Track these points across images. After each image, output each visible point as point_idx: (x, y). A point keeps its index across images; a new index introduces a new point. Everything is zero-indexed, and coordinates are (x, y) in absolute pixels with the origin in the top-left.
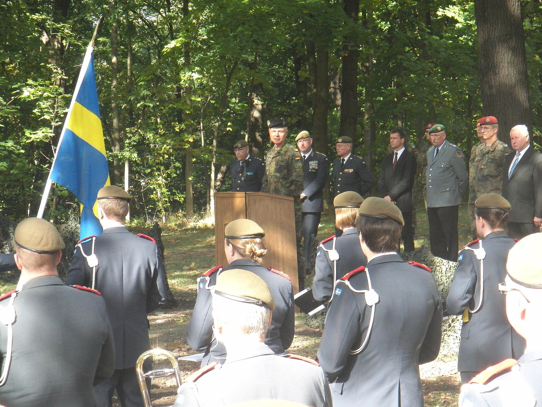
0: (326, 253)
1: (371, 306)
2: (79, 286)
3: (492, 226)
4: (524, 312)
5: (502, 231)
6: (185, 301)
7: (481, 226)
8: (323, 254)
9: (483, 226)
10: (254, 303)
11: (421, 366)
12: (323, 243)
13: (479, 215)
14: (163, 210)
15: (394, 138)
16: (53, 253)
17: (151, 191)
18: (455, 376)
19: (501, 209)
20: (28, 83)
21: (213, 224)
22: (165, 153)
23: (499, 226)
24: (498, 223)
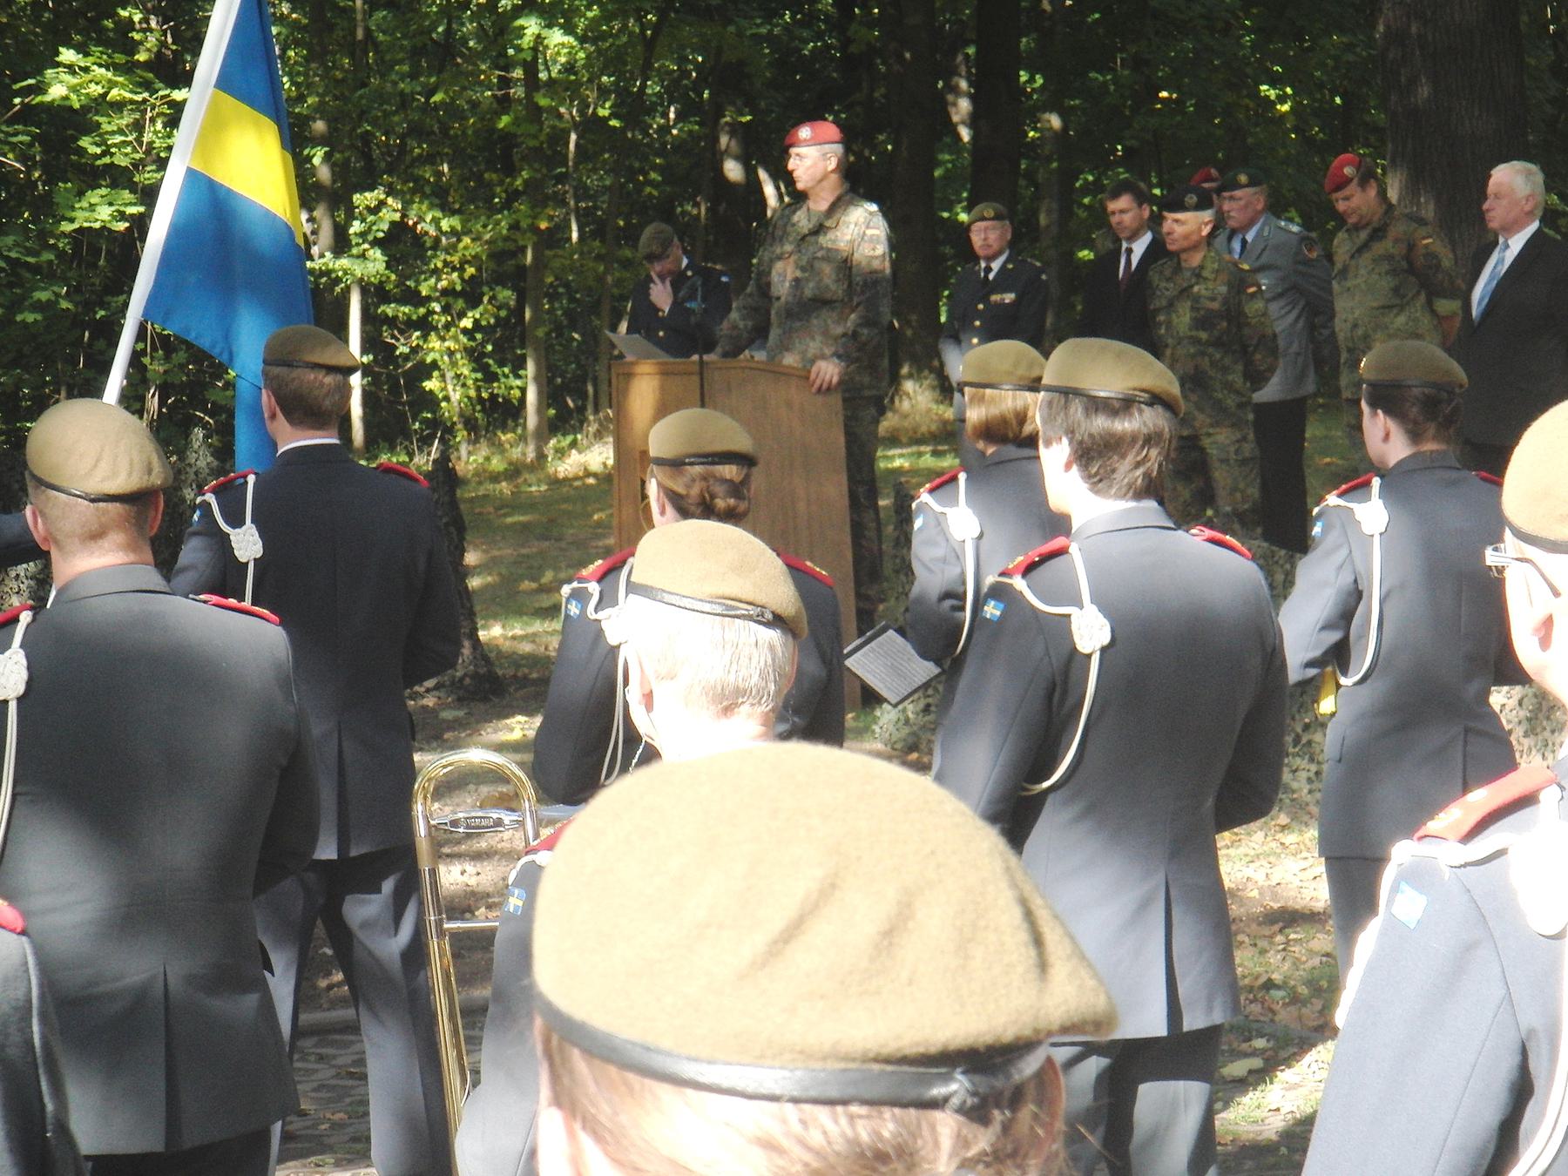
0: (941, 518)
1: (1089, 656)
2: (215, 598)
3: (1415, 436)
4: (1548, 623)
5: (1444, 452)
6: (525, 677)
7: (1381, 434)
8: (932, 522)
9: (1387, 437)
10: (749, 618)
11: (1224, 839)
12: (931, 491)
13: (1374, 405)
14: (459, 426)
15: (1122, 211)
16: (135, 499)
17: (427, 370)
18: (1314, 884)
19: (1434, 385)
20: (60, 59)
21: (605, 465)
22: (468, 262)
23: (1434, 438)
24: (1431, 431)
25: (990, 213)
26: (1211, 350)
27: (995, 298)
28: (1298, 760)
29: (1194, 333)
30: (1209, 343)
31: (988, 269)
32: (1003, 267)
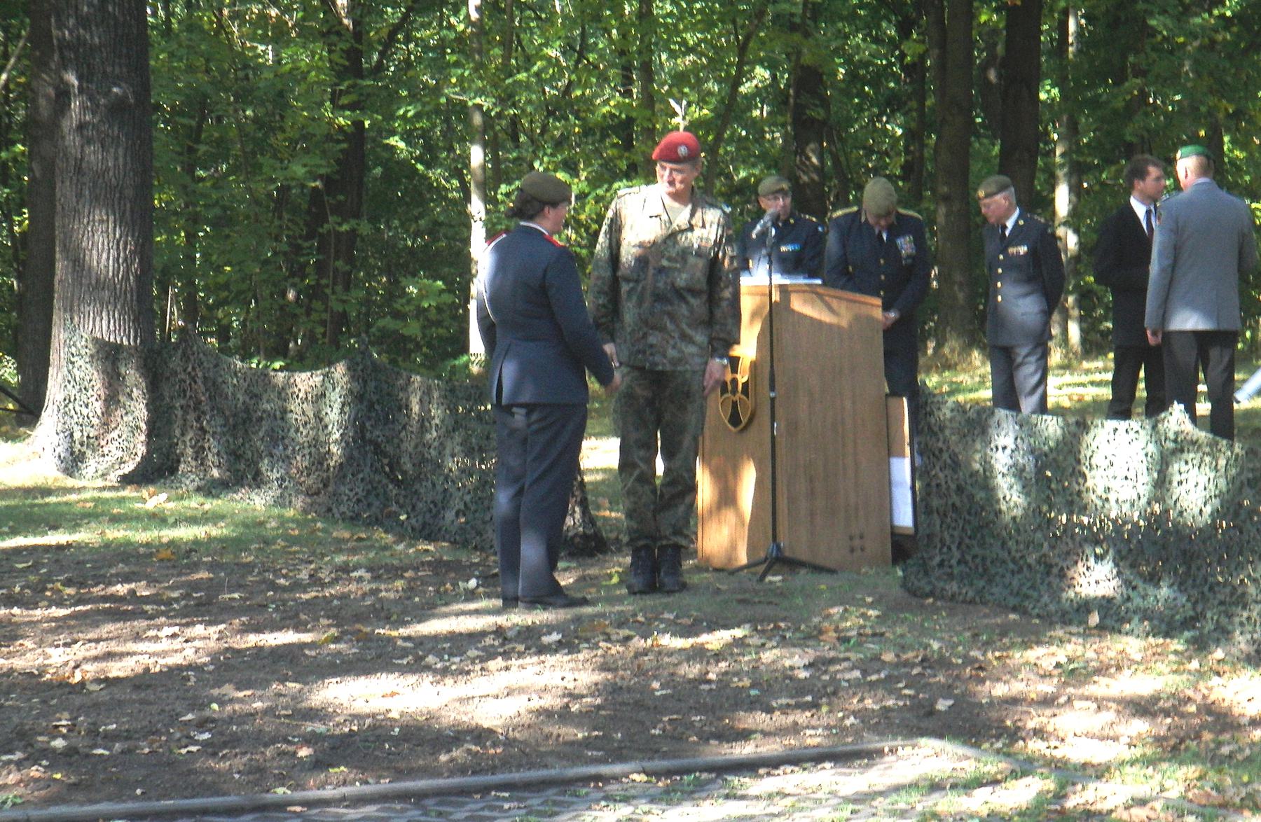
27: (1012, 250)
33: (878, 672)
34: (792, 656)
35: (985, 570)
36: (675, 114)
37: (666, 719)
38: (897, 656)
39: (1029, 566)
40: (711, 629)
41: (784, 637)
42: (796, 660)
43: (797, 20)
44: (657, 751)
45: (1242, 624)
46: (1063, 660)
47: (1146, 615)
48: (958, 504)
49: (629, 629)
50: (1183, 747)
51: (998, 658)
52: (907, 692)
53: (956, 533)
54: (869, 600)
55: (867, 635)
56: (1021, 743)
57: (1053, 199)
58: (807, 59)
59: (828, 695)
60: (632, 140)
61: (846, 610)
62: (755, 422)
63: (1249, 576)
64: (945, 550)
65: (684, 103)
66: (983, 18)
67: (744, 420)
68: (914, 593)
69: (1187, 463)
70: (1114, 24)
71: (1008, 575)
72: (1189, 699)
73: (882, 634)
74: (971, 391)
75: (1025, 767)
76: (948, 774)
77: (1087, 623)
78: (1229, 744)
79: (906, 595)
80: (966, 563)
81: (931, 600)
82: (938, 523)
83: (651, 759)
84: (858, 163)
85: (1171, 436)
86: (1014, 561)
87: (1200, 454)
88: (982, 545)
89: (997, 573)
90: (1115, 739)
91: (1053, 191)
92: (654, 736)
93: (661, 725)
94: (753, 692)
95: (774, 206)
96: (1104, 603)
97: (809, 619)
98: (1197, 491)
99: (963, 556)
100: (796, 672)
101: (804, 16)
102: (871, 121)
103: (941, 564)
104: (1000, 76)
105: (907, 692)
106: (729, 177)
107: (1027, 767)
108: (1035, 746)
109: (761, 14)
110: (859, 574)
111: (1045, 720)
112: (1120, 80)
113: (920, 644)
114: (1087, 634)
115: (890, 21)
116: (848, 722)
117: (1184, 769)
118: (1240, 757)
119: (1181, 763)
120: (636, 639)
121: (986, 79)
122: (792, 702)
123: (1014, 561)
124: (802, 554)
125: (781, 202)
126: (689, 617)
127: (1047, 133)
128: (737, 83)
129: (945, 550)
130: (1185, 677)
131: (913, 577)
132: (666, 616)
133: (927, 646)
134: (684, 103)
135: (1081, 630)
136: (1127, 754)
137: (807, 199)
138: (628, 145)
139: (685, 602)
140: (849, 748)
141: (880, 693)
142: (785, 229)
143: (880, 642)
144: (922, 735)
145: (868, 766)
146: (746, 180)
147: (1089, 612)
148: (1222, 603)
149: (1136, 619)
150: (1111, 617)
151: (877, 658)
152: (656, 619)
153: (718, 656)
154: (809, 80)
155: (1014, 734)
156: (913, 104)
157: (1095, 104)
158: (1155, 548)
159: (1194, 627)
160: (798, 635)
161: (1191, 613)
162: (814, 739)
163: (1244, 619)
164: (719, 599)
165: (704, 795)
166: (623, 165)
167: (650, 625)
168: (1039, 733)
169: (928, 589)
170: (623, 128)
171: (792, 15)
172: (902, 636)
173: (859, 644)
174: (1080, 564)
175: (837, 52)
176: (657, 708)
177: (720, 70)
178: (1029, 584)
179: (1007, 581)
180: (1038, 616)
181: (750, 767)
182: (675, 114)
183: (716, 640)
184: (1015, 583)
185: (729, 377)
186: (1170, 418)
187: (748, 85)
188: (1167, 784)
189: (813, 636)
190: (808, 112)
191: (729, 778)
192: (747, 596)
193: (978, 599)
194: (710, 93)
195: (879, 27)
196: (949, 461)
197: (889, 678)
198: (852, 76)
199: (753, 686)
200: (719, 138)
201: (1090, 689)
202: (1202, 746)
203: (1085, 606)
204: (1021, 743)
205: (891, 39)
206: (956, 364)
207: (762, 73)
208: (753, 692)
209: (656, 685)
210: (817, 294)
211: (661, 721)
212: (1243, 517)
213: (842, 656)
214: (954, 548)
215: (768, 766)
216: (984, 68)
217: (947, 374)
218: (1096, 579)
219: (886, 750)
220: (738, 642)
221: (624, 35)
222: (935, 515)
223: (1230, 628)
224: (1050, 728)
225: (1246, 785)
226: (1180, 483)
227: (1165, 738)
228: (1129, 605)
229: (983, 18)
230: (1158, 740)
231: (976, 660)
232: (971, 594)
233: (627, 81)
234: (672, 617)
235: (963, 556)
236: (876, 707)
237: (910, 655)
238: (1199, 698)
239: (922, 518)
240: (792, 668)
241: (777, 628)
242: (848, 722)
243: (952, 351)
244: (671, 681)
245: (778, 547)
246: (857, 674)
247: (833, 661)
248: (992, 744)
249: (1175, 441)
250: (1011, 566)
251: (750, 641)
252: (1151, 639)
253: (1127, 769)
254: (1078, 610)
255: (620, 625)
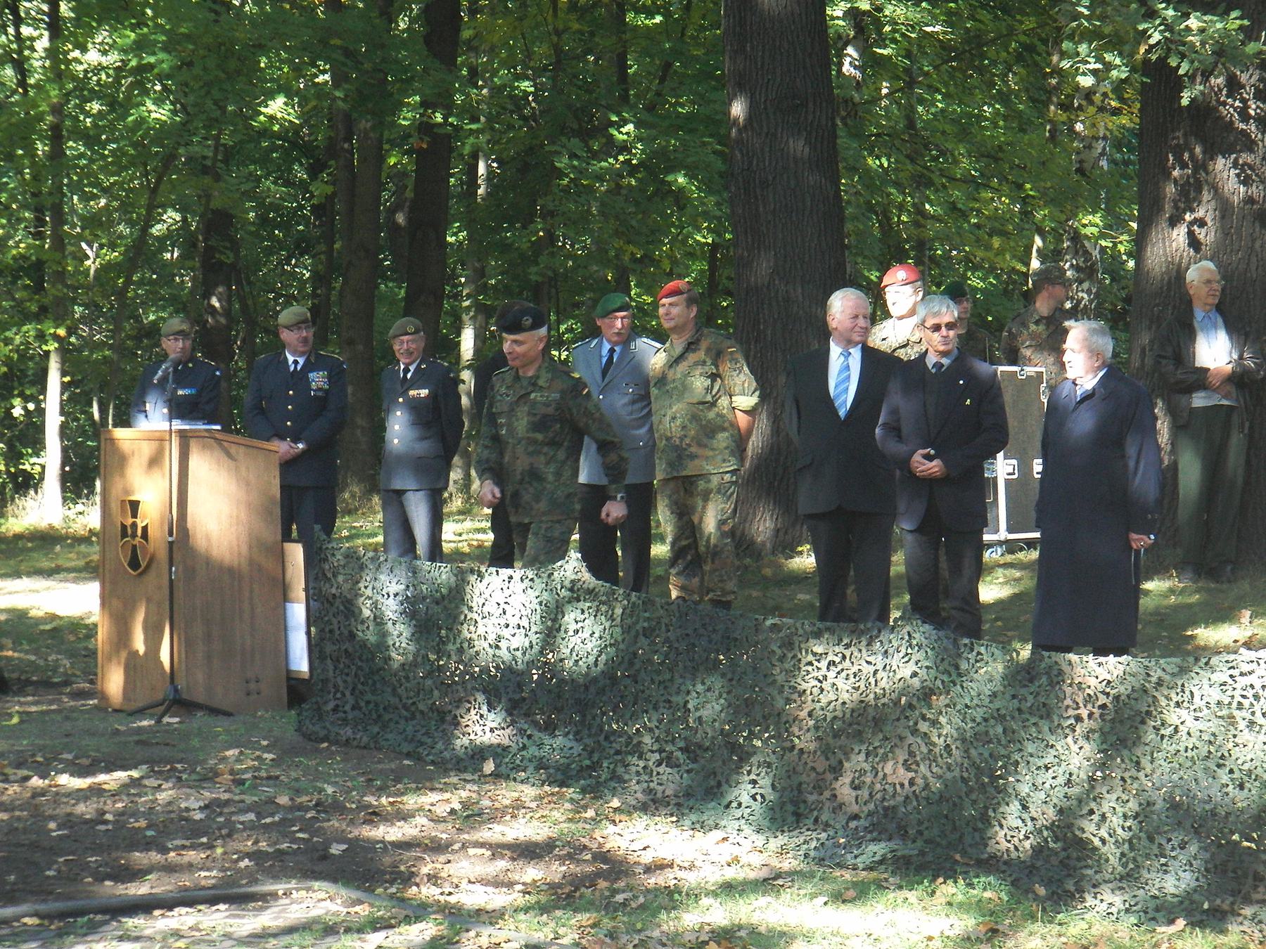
25: (411, 329)
26: (545, 449)
27: (412, 393)
28: (630, 758)
29: (531, 435)
30: (544, 444)
31: (406, 370)
32: (418, 368)
33: (272, 815)
34: (187, 799)
35: (379, 716)
36: (88, 257)
37: (61, 860)
38: (291, 799)
39: (422, 712)
40: (109, 770)
41: (180, 779)
42: (194, 803)
43: (209, 163)
44: (51, 893)
45: (638, 773)
46: (457, 806)
47: (541, 765)
48: (350, 650)
49: (28, 769)
50: (577, 894)
51: (391, 804)
52: (301, 835)
53: (349, 679)
54: (265, 743)
55: (261, 778)
56: (414, 888)
57: (459, 343)
58: (216, 204)
59: (222, 837)
60: (44, 281)
61: (241, 753)
62: (154, 566)
63: (645, 727)
64: (339, 695)
65: (96, 245)
66: (392, 161)
67: (143, 564)
68: (309, 737)
69: (583, 612)
70: (525, 169)
71: (403, 722)
72: (585, 847)
73: (277, 777)
74: (369, 536)
75: (419, 912)
76: (341, 918)
77: (481, 770)
78: (624, 892)
79: (301, 739)
80: (360, 709)
81: (325, 745)
82: (331, 668)
83: (44, 901)
84: (266, 306)
85: (567, 583)
86: (405, 707)
87: (597, 603)
88: (374, 692)
89: (391, 720)
90: (510, 885)
91: (459, 335)
92: (48, 877)
93: (55, 867)
94: (149, 833)
95: (174, 347)
96: (499, 750)
97: (205, 761)
98: (585, 639)
99: (357, 702)
100: (192, 813)
101: (215, 159)
102: (280, 263)
103: (335, 710)
104: (409, 220)
105: (301, 835)
106: (138, 319)
107: (418, 913)
108: (428, 892)
109: (173, 157)
110: (255, 717)
111: (439, 866)
112: (528, 220)
113: (315, 788)
114: (483, 779)
115: (301, 164)
116: (242, 864)
117: (579, 917)
118: (634, 905)
119: (575, 911)
120: (35, 778)
121: (395, 223)
122: (187, 843)
123: (405, 707)
124: (200, 697)
125: (180, 344)
126: (88, 757)
127: (455, 276)
128: (148, 225)
129: (339, 695)
130: (581, 825)
131: (307, 722)
132: (65, 756)
133: (321, 790)
134: (96, 245)
135: (476, 777)
136: (521, 900)
137: (211, 341)
138: (39, 288)
139: (84, 743)
140: (243, 890)
141: (274, 835)
142: (181, 376)
143: (275, 786)
144: (316, 879)
145: (262, 909)
146: (154, 323)
147: (484, 759)
148: (618, 753)
149: (531, 769)
150: (505, 764)
151: (271, 801)
152: (55, 759)
153: (115, 795)
154: (219, 223)
155: (408, 879)
156: (323, 247)
157: (505, 247)
158: (531, 693)
159: (590, 776)
160: (194, 777)
161: (587, 762)
162: (207, 877)
163: (639, 769)
164: (117, 739)
165: (96, 937)
166: (34, 308)
167: (48, 765)
168: (433, 879)
169: (322, 733)
170: (34, 269)
171: (205, 158)
172: (297, 780)
173: (255, 787)
174: (473, 712)
175: (248, 195)
176: (54, 849)
177: (131, 213)
178: (424, 731)
179: (401, 727)
180: (433, 763)
181: (145, 907)
182: (88, 257)
183: (113, 779)
184: (410, 729)
185: (130, 521)
186: (566, 566)
187: (159, 227)
188: (561, 931)
189: (210, 778)
190: (217, 256)
191: (124, 920)
192: (144, 737)
193: (372, 745)
194: (121, 236)
195: (290, 170)
196: (342, 608)
197: (283, 820)
198: (263, 220)
199: (149, 827)
200: (128, 282)
201: (484, 834)
202: (597, 893)
203: (479, 754)
204: (414, 888)
205: (301, 180)
206: (357, 510)
207: (172, 216)
208: (149, 833)
209: (52, 825)
210: (216, 439)
211: (56, 862)
212: (637, 667)
213: (237, 798)
214: (348, 693)
215: (162, 908)
216: (392, 211)
217: (347, 519)
218: (483, 726)
219: (280, 893)
220: (134, 782)
221: (35, 177)
222: (329, 661)
223: (626, 777)
224: (444, 874)
225: (640, 931)
226: (576, 632)
227: (559, 886)
228: (524, 753)
229: (392, 161)
230: (553, 886)
231: (370, 806)
232: (365, 739)
233: (40, 221)
234: (70, 757)
235: (357, 702)
236: (271, 850)
237: (305, 798)
238: (594, 846)
239: (317, 662)
240: (187, 809)
241: (173, 769)
242: (242, 864)
243: (353, 496)
244: (69, 821)
245: (176, 690)
246: (251, 816)
247: (227, 803)
248: (386, 889)
249: (571, 590)
250: (405, 713)
251: (146, 782)
252: (547, 788)
253: (522, 916)
254: (472, 757)
255: (19, 766)
